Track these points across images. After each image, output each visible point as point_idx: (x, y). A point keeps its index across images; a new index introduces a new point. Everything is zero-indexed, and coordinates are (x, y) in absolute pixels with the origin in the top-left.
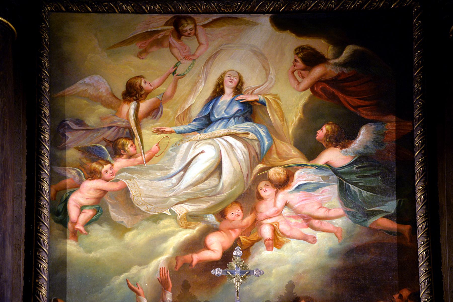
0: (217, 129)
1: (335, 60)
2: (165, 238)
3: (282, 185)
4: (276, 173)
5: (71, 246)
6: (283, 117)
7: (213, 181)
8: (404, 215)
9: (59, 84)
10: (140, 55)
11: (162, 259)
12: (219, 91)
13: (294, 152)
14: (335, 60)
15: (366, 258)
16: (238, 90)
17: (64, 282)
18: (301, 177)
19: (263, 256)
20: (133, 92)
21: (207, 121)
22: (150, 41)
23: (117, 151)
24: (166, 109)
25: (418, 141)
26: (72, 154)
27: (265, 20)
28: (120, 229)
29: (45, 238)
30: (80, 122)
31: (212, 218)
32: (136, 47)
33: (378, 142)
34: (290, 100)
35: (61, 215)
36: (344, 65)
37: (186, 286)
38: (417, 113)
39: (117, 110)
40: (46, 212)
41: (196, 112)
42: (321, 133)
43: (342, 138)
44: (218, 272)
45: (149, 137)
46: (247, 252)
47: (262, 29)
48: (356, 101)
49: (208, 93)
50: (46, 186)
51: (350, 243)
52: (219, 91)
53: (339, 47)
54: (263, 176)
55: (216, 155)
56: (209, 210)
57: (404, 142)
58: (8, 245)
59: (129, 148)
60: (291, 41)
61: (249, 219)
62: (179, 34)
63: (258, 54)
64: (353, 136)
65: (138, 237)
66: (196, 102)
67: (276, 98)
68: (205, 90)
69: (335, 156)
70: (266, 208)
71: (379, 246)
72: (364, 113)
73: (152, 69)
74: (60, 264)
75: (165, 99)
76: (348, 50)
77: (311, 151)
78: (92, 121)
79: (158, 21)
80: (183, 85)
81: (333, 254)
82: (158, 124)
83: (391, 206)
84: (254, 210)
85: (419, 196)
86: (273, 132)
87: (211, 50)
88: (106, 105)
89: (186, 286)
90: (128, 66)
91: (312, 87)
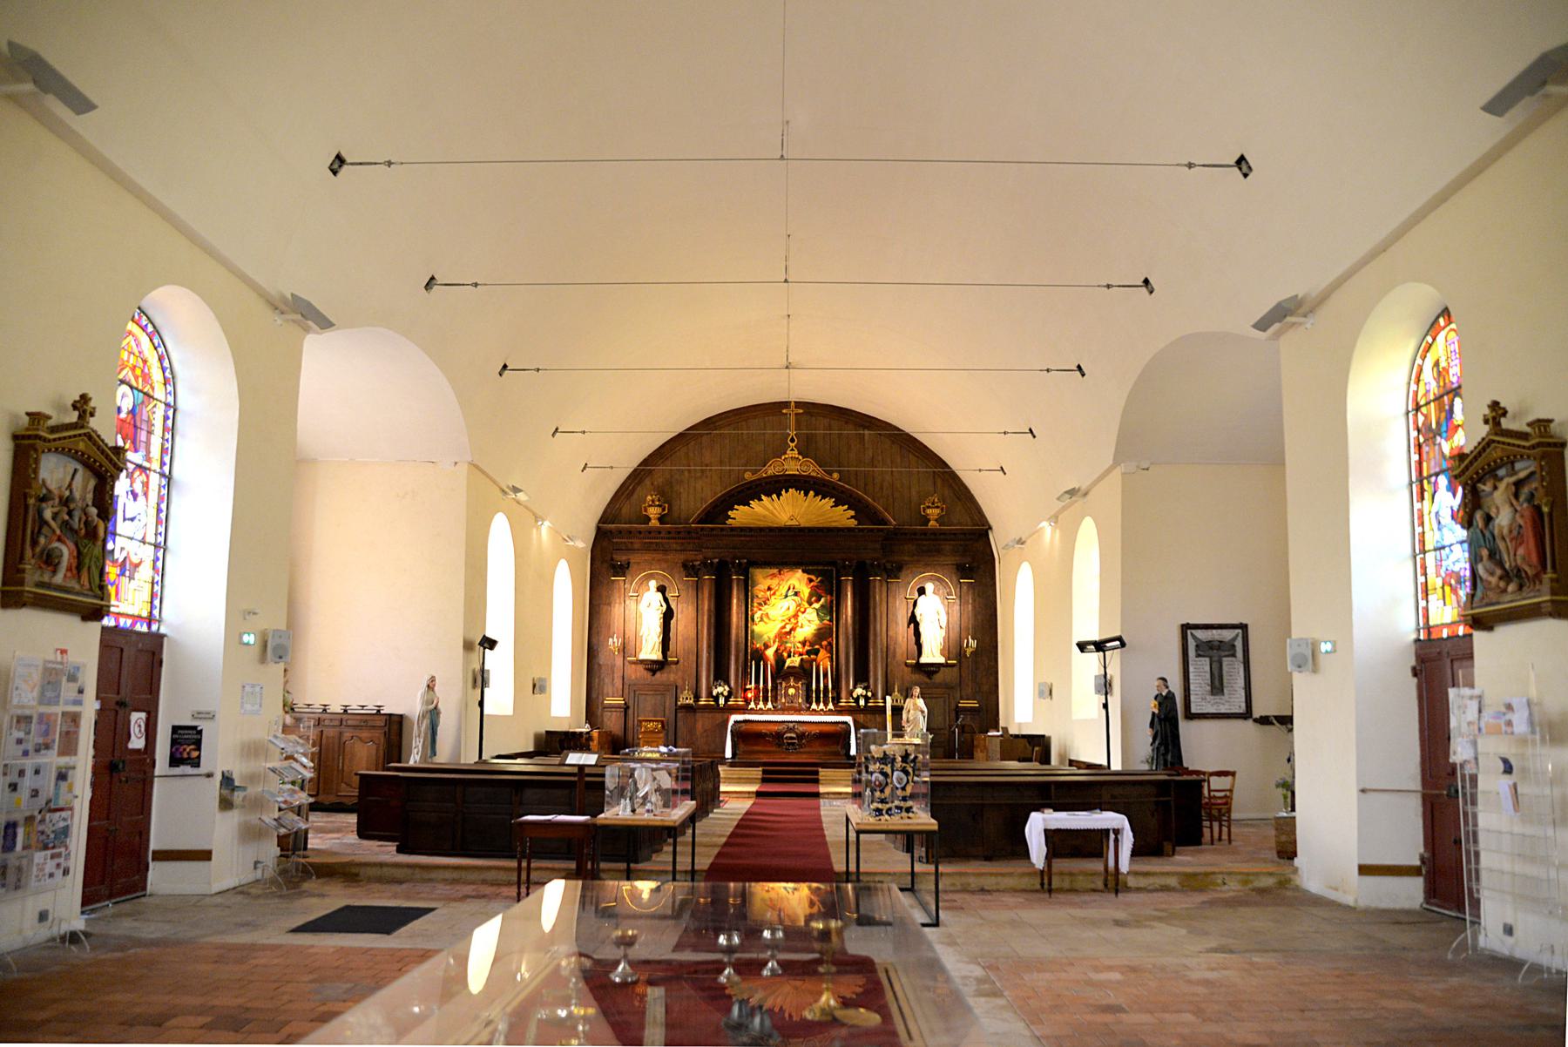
1: (817, 580)
11: (1102, 933)
14: (817, 580)
22: (773, 576)
34: (806, 591)
43: (818, 601)
47: (799, 573)
55: (791, 602)
58: (1441, 986)
65: (771, 624)
69: (817, 606)
73: (774, 583)
90: (768, 582)
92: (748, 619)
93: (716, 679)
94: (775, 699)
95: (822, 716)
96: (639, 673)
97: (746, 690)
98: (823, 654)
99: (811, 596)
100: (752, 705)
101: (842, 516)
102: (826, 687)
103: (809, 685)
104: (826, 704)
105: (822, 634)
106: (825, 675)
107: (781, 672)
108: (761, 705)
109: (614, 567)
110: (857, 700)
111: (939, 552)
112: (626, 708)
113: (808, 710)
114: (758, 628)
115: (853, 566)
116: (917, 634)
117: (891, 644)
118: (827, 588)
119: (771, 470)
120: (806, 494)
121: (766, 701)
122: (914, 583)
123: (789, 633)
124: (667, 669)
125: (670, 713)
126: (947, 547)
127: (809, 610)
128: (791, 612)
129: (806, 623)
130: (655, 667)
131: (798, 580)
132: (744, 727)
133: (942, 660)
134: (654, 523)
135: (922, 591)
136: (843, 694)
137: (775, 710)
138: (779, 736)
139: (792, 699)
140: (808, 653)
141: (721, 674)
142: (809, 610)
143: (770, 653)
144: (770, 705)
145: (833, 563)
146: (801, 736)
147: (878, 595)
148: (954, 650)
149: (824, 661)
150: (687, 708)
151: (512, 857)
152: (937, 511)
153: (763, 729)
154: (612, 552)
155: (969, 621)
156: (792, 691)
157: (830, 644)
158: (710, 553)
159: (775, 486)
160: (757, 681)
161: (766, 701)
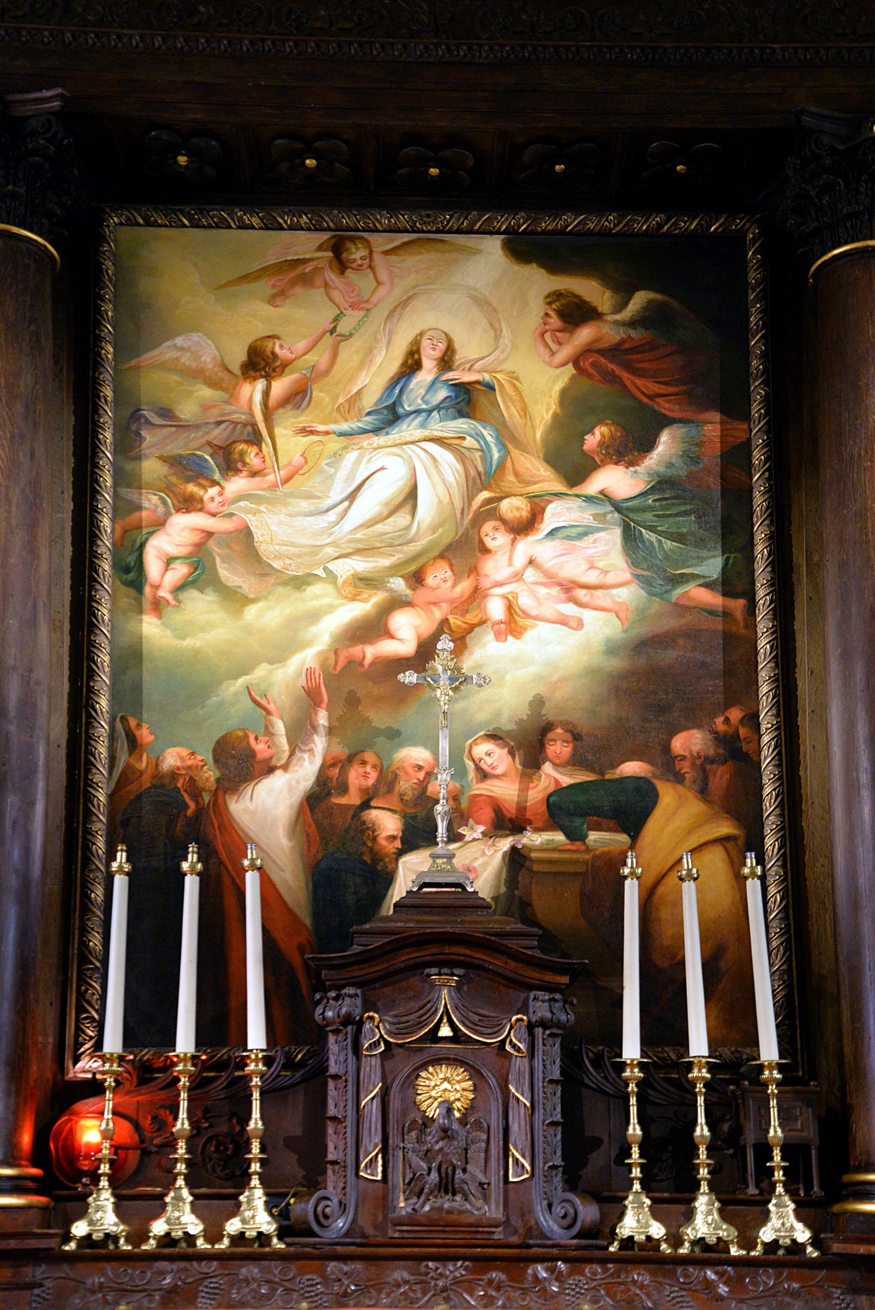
0: (408, 430)
2: (314, 616)
3: (523, 528)
4: (513, 507)
5: (150, 628)
6: (525, 411)
7: (401, 519)
8: (735, 582)
9: (129, 349)
10: (272, 300)
12: (412, 365)
13: (544, 471)
15: (670, 656)
16: (446, 362)
17: (138, 687)
18: (557, 514)
19: (487, 652)
20: (259, 363)
21: (390, 415)
22: (291, 276)
23: (231, 465)
24: (318, 393)
25: (758, 456)
26: (151, 468)
27: (493, 245)
28: (236, 600)
29: (104, 611)
30: (166, 413)
31: (398, 584)
32: (265, 286)
33: (690, 457)
34: (537, 382)
35: (132, 573)
36: (632, 324)
37: (353, 701)
38: (756, 409)
39: (232, 394)
40: (106, 566)
41: (370, 400)
42: (592, 441)
43: (631, 447)
45: (289, 442)
46: (461, 643)
48: (653, 387)
49: (393, 367)
50: (106, 522)
51: (643, 630)
52: (412, 365)
54: (489, 511)
55: (417, 470)
56: (393, 570)
57: (735, 456)
59: (252, 458)
60: (538, 282)
61: (465, 586)
64: (648, 445)
65: (267, 614)
67: (513, 377)
68: (388, 361)
69: (618, 480)
70: (495, 568)
71: (691, 634)
72: (665, 407)
73: (295, 324)
74: (131, 657)
75: (315, 375)
77: (575, 470)
78: (187, 411)
79: (306, 244)
80: (349, 353)
82: (303, 419)
83: (713, 566)
84: (474, 570)
85: (761, 549)
86: (507, 436)
87: (397, 293)
89: (353, 701)
90: (253, 318)
91: (576, 361)
94: (301, 1166)
98: (678, 819)
99: (575, 413)
100: (103, 1215)
104: (743, 1206)
105: (653, 685)
107: (353, 936)
114: (176, 629)
121: (219, 1185)
131: (483, 311)
139: (445, 1155)
140: (562, 811)
143: (267, 809)
144: (255, 1215)
151: (199, 1044)
156: (443, 1089)
157: (736, 752)
160: (150, 1018)
161: (219, 1185)
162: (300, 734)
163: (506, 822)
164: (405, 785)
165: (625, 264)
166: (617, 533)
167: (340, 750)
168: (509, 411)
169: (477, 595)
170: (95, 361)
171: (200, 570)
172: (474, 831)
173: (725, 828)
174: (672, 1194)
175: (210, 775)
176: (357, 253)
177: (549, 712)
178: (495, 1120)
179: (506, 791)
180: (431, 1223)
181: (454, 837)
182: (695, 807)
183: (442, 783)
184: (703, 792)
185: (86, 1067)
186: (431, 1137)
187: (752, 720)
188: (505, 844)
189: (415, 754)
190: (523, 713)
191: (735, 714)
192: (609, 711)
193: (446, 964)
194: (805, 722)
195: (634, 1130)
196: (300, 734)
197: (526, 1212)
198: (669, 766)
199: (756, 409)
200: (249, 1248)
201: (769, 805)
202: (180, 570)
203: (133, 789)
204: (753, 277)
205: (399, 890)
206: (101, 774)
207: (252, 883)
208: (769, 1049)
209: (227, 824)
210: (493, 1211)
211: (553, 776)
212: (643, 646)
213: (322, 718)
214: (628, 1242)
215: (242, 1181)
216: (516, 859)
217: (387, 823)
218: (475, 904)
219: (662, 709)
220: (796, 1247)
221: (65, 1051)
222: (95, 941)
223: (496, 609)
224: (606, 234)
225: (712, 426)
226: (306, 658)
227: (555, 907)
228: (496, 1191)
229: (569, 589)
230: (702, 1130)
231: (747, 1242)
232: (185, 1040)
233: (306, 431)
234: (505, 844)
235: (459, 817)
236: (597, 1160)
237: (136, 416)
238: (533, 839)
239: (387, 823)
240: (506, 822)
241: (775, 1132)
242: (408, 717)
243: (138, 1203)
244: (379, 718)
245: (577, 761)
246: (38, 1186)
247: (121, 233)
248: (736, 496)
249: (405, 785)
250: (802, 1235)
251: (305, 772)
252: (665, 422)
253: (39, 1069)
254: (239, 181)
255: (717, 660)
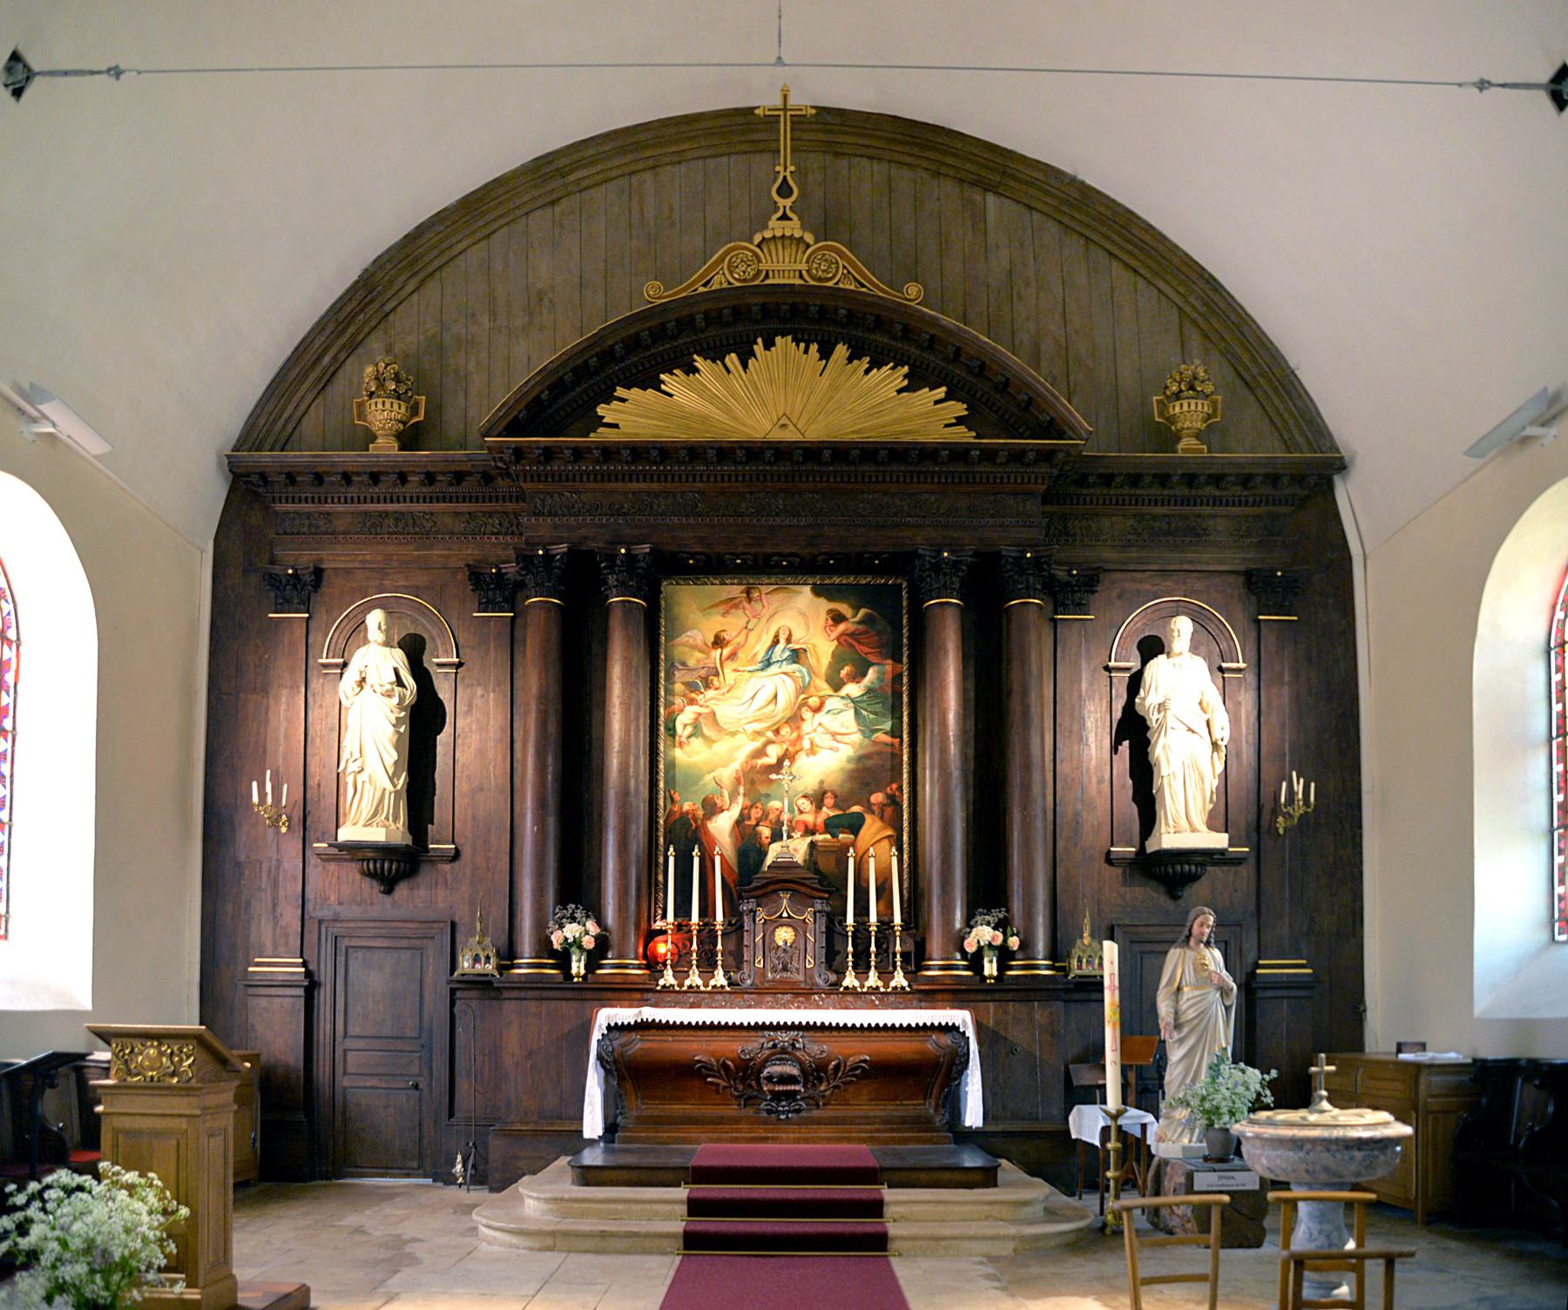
0: (774, 669)
1: (854, 617)
2: (738, 748)
3: (817, 710)
4: (814, 701)
5: (678, 754)
6: (818, 660)
7: (771, 707)
8: (895, 732)
9: (669, 638)
10: (723, 615)
12: (776, 642)
13: (825, 685)
15: (870, 763)
16: (789, 640)
17: (674, 777)
18: (831, 703)
19: (802, 761)
20: (719, 642)
21: (768, 663)
22: (730, 605)
23: (708, 686)
24: (741, 654)
25: (905, 680)
26: (678, 687)
27: (807, 589)
28: (709, 741)
29: (661, 747)
30: (684, 664)
31: (770, 734)
32: (721, 609)
33: (880, 679)
34: (823, 648)
35: (672, 731)
36: (859, 623)
37: (753, 782)
38: (905, 660)
39: (708, 654)
40: (662, 728)
41: (760, 657)
42: (843, 673)
43: (858, 675)
44: (773, 776)
45: (729, 674)
46: (792, 759)
48: (867, 650)
49: (769, 643)
50: (662, 711)
51: (861, 752)
52: (776, 642)
53: (856, 609)
54: (804, 704)
55: (780, 684)
56: (768, 728)
57: (897, 678)
59: (716, 682)
60: (824, 605)
61: (795, 735)
62: (750, 600)
63: (803, 614)
64: (864, 675)
65: (722, 746)
66: (760, 649)
67: (814, 646)
68: (767, 640)
69: (853, 689)
70: (806, 727)
71: (879, 753)
72: (871, 658)
73: (731, 625)
74: (671, 765)
75: (740, 646)
76: (862, 612)
77: (837, 685)
78: (691, 663)
79: (736, 590)
80: (752, 637)
81: (849, 761)
82: (735, 665)
83: (888, 726)
84: (798, 728)
85: (905, 719)
86: (811, 671)
87: (771, 611)
88: (701, 651)
89: (753, 782)
91: (838, 639)
92: (656, 728)
93: (563, 899)
94: (736, 960)
95: (874, 1012)
96: (341, 890)
97: (652, 935)
98: (872, 828)
99: (837, 661)
100: (668, 978)
101: (930, 416)
102: (885, 924)
103: (834, 919)
104: (885, 974)
105: (869, 774)
106: (884, 890)
107: (752, 879)
108: (695, 979)
109: (275, 582)
110: (975, 962)
111: (1195, 534)
112: (311, 986)
113: (837, 994)
114: (688, 754)
115: (971, 551)
116: (1143, 772)
117: (1066, 811)
118: (890, 634)
119: (725, 272)
120: (825, 354)
121: (707, 965)
122: (1134, 624)
123: (778, 767)
124: (426, 875)
125: (436, 1006)
126: (1220, 521)
127: (833, 703)
128: (782, 708)
129: (823, 740)
130: (393, 866)
131: (802, 617)
132: (639, 1045)
133: (1220, 841)
134: (386, 447)
135: (1152, 647)
136: (935, 944)
137: (736, 993)
138: (745, 1073)
140: (831, 826)
141: (575, 885)
142: (833, 703)
143: (721, 827)
144: (719, 979)
145: (900, 562)
146: (815, 1072)
147: (1036, 644)
148: (1246, 806)
149: (876, 850)
150: (481, 984)
152: (1204, 407)
153: (699, 1050)
154: (274, 539)
155: (1279, 733)
156: (784, 935)
157: (894, 801)
158: (540, 528)
159: (734, 324)
160: (683, 908)
161: (707, 965)
162: (733, 795)
163: (810, 831)
164: (772, 817)
165: (860, 597)
166: (852, 712)
167: (748, 803)
168: (812, 660)
169: (800, 737)
170: (658, 643)
171: (696, 731)
172: (797, 835)
173: (889, 832)
174: (862, 968)
175: (700, 813)
176: (755, 594)
177: (826, 786)
178: (802, 947)
179: (809, 818)
180: (780, 982)
181: (789, 837)
182: (879, 824)
183: (785, 817)
184: (882, 818)
185: (658, 925)
186: (780, 952)
187: (900, 788)
188: (809, 839)
189: (775, 804)
190: (816, 787)
191: (894, 786)
192: (848, 785)
193: (785, 890)
194: (919, 788)
195: (850, 949)
196: (733, 795)
197: (812, 978)
198: (869, 808)
199: (905, 660)
200: (718, 990)
201: (906, 824)
202: (689, 730)
203: (672, 819)
204: (905, 603)
205: (769, 861)
206: (661, 813)
207: (718, 860)
208: (897, 919)
209: (707, 832)
210: (801, 978)
211: (827, 812)
212: (861, 758)
213: (741, 790)
214: (847, 988)
215: (715, 966)
216: (812, 845)
217: (765, 832)
218: (794, 866)
219: (868, 784)
220: (903, 988)
221: (650, 919)
222: (661, 878)
223: (806, 744)
224: (849, 585)
225: (888, 666)
226: (736, 765)
227: (826, 864)
228: (802, 970)
229: (834, 735)
230: (873, 948)
231: (886, 985)
232: (695, 918)
233: (736, 670)
234: (809, 839)
235: (792, 829)
236: (839, 958)
237: (673, 665)
238: (819, 837)
239: (765, 832)
240: (810, 831)
241: (898, 948)
242: (773, 789)
243: (681, 974)
244: (763, 790)
245: (836, 806)
246: (647, 967)
247: (667, 588)
248: (897, 695)
249: (772, 817)
250: (905, 983)
251: (734, 813)
252: (871, 664)
253: (644, 925)
254: (711, 566)
255: (888, 765)
